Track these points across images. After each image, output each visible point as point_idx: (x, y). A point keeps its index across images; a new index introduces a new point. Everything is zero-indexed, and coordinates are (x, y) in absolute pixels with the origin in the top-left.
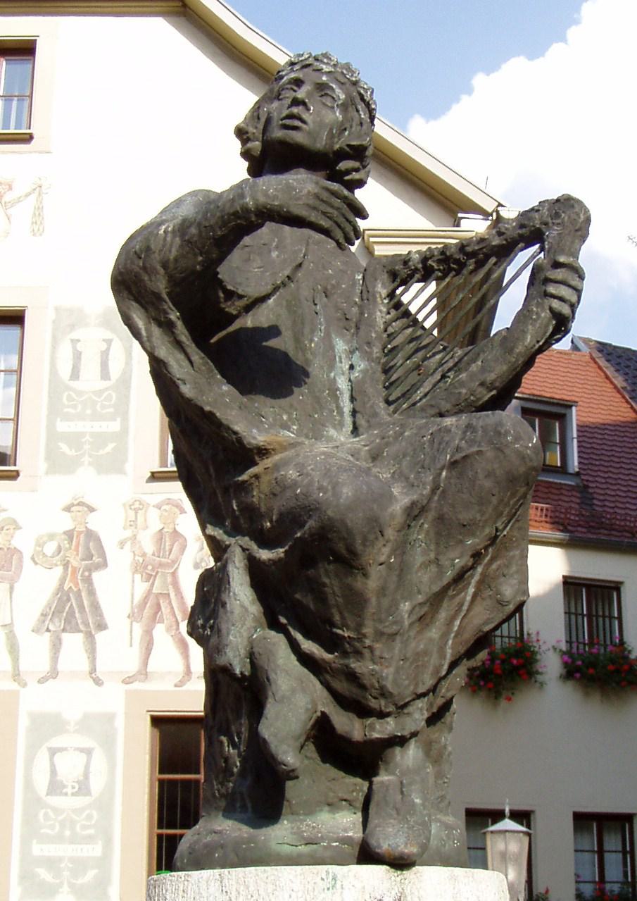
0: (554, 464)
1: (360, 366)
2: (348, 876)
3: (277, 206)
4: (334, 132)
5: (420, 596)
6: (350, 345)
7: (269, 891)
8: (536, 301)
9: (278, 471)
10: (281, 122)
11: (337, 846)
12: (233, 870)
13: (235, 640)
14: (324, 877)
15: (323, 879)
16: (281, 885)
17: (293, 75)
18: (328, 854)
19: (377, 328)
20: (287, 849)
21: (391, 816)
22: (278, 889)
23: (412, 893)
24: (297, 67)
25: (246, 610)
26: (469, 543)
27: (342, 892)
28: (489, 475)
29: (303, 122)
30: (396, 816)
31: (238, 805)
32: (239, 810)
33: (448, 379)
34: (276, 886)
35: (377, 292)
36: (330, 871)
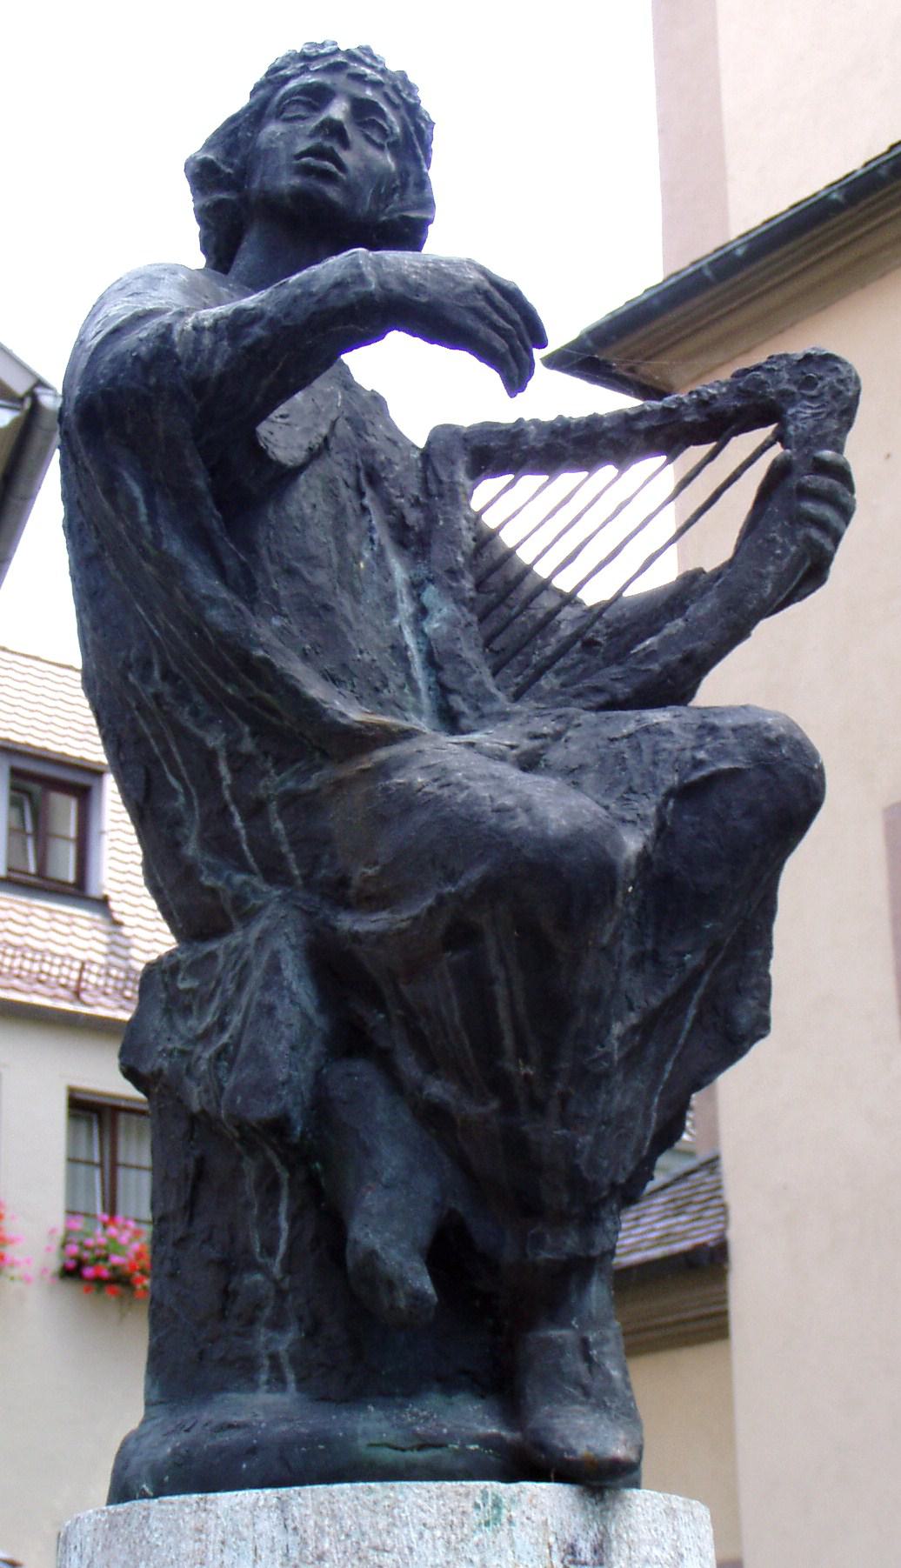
0: (21, 867)
1: (440, 610)
2: (519, 1500)
3: (424, 304)
4: (383, 190)
5: (632, 1015)
6: (412, 572)
7: (380, 1526)
8: (779, 525)
9: (388, 776)
10: (295, 162)
11: (476, 1450)
12: (308, 1490)
13: (296, 1073)
14: (479, 1502)
15: (477, 1506)
16: (403, 1515)
17: (309, 79)
18: (460, 1464)
19: (465, 548)
20: (388, 1455)
21: (574, 1400)
22: (398, 1523)
23: (620, 1536)
24: (316, 66)
25: (311, 1022)
26: (708, 926)
27: (510, 1530)
28: (748, 814)
29: (341, 165)
30: (582, 1398)
31: (263, 1377)
32: (265, 1387)
33: (598, 647)
34: (393, 1517)
35: (458, 483)
36: (489, 1491)
